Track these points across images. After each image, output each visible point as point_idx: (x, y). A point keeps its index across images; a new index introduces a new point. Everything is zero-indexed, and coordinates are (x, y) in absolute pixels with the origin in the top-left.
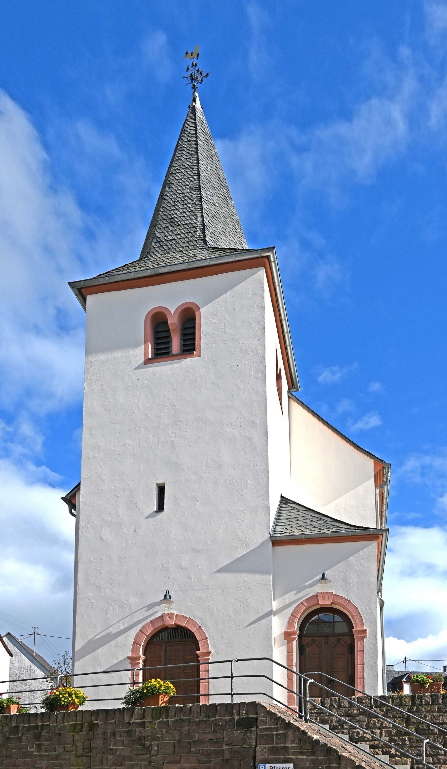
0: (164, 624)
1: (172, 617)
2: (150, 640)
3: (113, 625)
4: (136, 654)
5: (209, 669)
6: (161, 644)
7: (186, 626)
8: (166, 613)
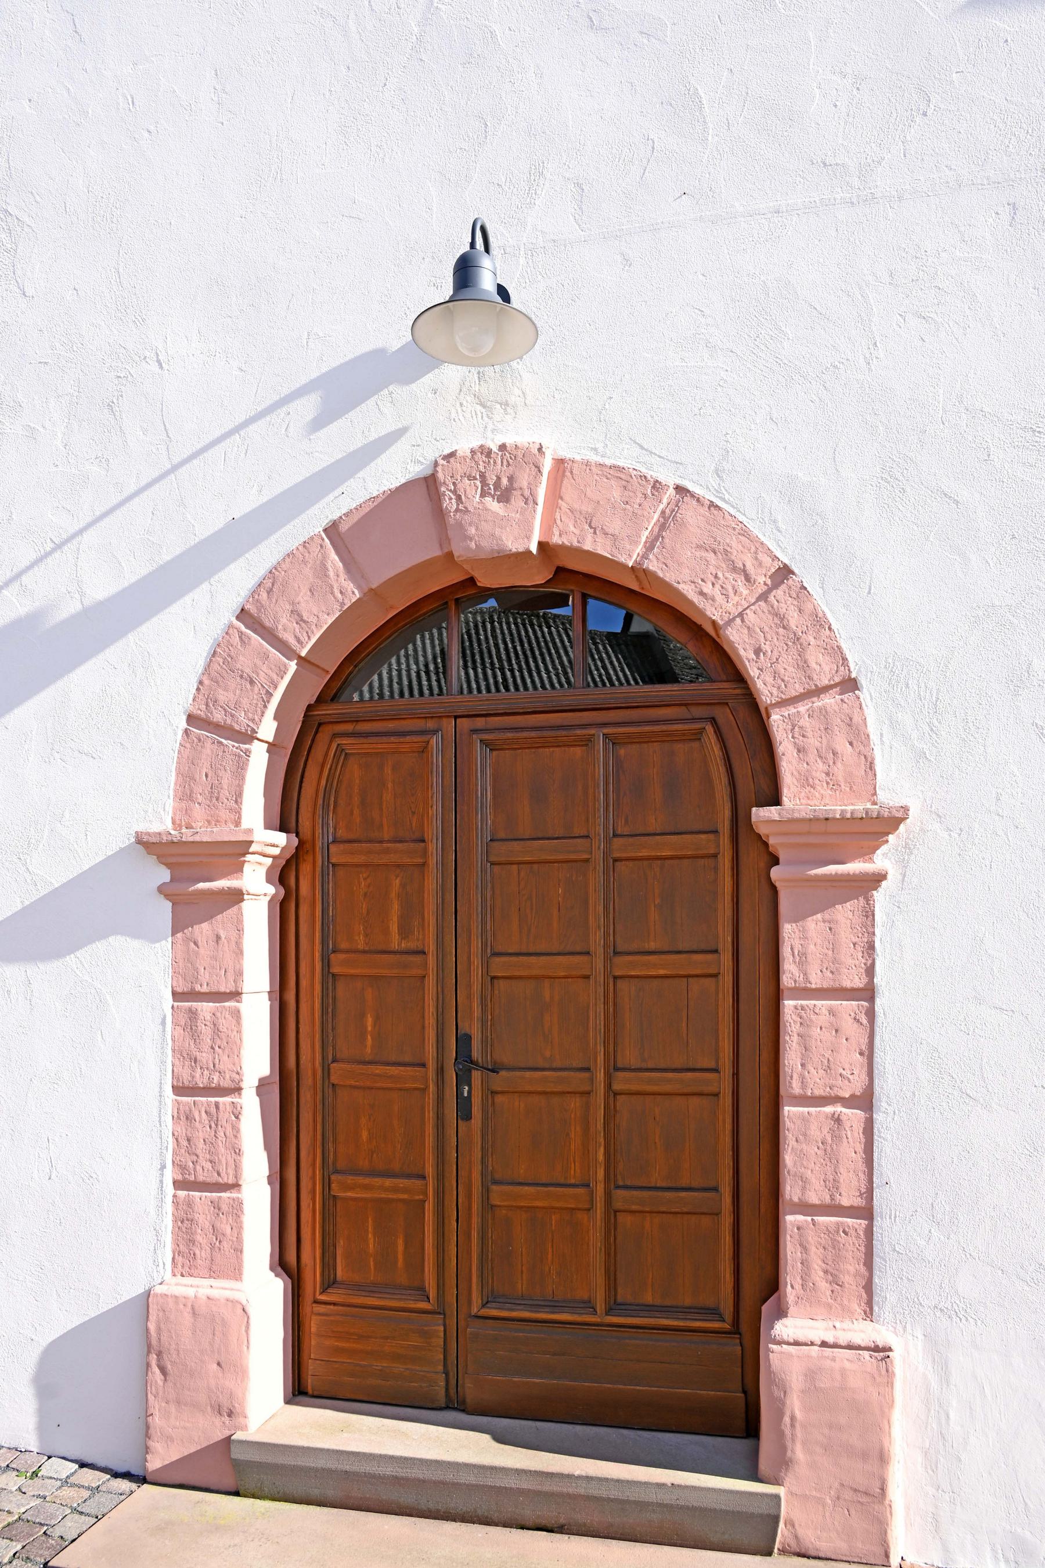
0: (450, 555)
1: (523, 481)
2: (330, 694)
3: (29, 568)
4: (213, 820)
5: (870, 971)
6: (419, 724)
7: (653, 565)
8: (464, 446)
